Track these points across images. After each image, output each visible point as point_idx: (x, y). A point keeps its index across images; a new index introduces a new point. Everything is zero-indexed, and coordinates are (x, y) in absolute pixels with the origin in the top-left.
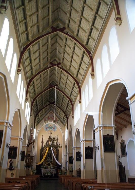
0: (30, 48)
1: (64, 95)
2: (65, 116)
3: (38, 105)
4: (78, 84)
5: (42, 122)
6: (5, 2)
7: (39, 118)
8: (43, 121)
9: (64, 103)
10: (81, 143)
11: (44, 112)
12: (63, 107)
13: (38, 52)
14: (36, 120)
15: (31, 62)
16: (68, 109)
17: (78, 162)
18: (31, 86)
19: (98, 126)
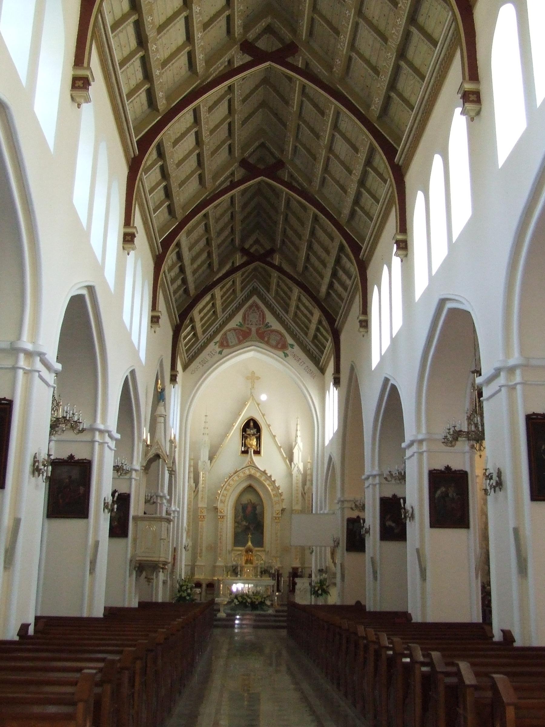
1: (319, 213)
2: (325, 323)
3: (189, 271)
5: (211, 355)
6: (85, 65)
7: (195, 335)
8: (212, 347)
9: (319, 258)
10: (408, 453)
11: (219, 302)
12: (315, 274)
13: (180, 24)
14: (182, 343)
17: (392, 546)
19: (497, 365)
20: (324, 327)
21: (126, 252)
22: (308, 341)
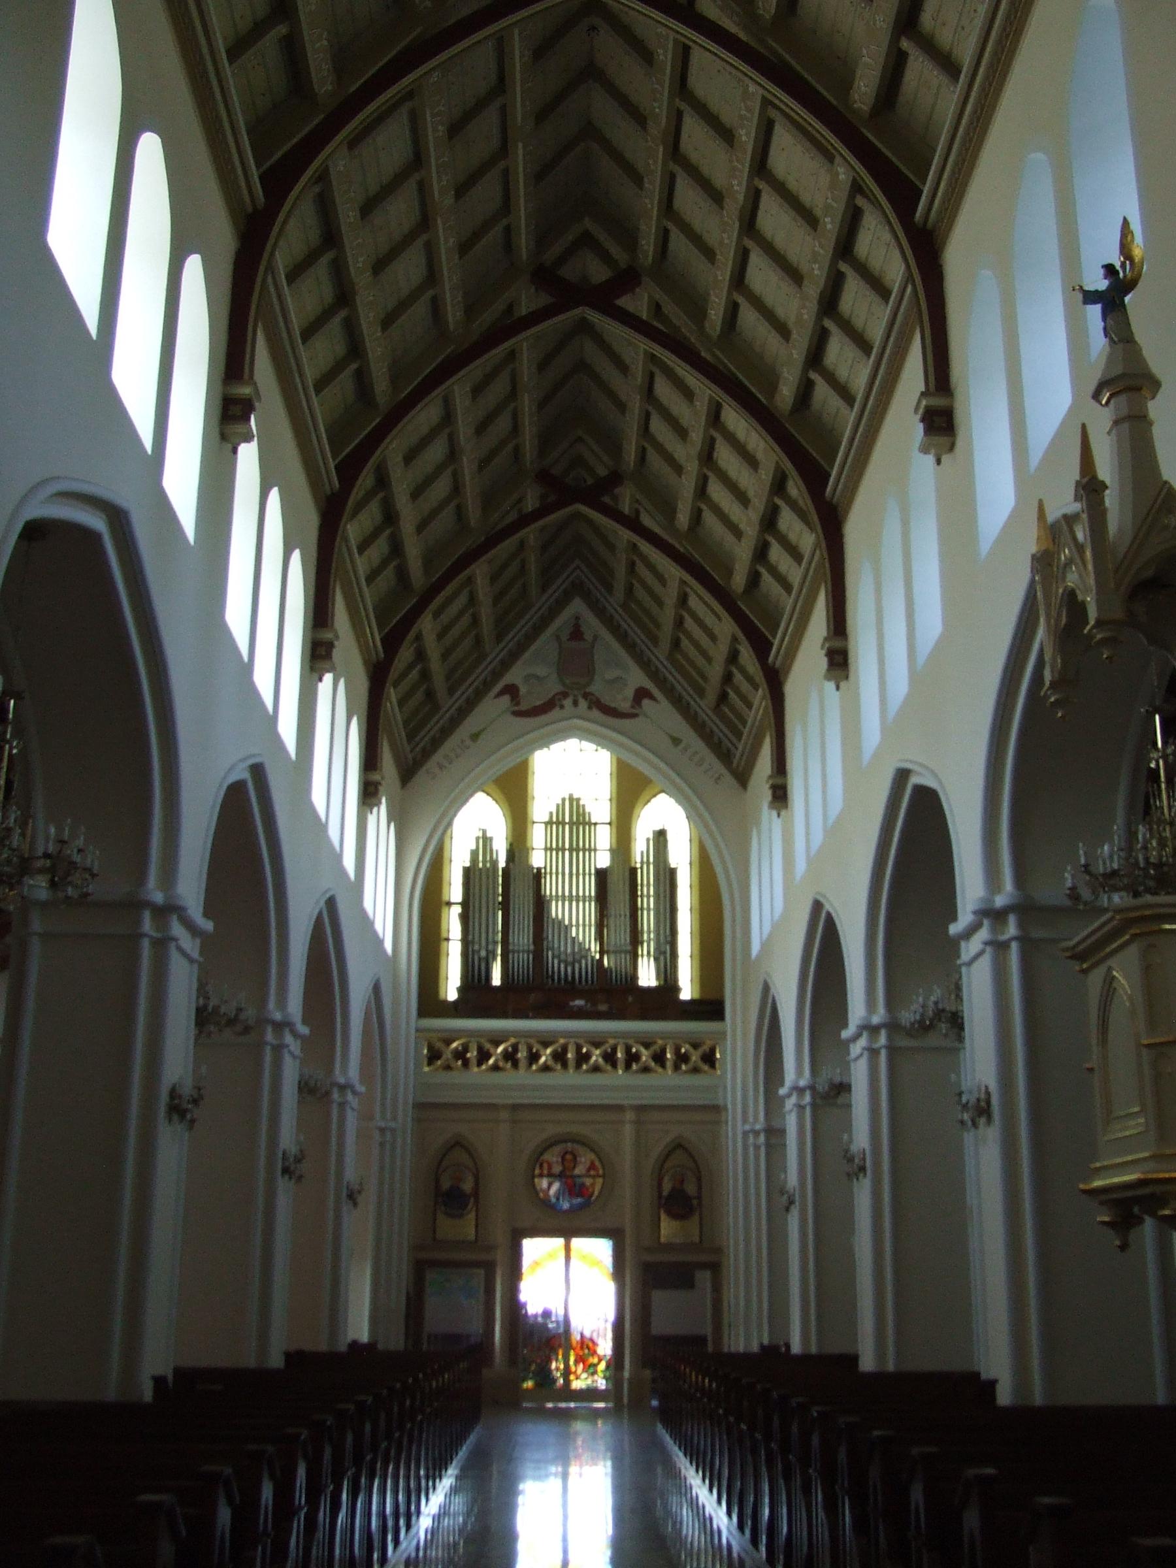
0: (327, 169)
2: (796, 488)
4: (818, 478)
6: (246, 376)
11: (486, 613)
15: (344, 297)
16: (776, 553)
18: (360, 506)
20: (793, 505)
21: (230, 446)
22: (704, 706)
